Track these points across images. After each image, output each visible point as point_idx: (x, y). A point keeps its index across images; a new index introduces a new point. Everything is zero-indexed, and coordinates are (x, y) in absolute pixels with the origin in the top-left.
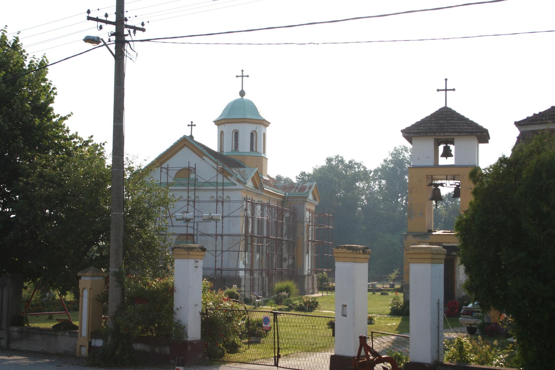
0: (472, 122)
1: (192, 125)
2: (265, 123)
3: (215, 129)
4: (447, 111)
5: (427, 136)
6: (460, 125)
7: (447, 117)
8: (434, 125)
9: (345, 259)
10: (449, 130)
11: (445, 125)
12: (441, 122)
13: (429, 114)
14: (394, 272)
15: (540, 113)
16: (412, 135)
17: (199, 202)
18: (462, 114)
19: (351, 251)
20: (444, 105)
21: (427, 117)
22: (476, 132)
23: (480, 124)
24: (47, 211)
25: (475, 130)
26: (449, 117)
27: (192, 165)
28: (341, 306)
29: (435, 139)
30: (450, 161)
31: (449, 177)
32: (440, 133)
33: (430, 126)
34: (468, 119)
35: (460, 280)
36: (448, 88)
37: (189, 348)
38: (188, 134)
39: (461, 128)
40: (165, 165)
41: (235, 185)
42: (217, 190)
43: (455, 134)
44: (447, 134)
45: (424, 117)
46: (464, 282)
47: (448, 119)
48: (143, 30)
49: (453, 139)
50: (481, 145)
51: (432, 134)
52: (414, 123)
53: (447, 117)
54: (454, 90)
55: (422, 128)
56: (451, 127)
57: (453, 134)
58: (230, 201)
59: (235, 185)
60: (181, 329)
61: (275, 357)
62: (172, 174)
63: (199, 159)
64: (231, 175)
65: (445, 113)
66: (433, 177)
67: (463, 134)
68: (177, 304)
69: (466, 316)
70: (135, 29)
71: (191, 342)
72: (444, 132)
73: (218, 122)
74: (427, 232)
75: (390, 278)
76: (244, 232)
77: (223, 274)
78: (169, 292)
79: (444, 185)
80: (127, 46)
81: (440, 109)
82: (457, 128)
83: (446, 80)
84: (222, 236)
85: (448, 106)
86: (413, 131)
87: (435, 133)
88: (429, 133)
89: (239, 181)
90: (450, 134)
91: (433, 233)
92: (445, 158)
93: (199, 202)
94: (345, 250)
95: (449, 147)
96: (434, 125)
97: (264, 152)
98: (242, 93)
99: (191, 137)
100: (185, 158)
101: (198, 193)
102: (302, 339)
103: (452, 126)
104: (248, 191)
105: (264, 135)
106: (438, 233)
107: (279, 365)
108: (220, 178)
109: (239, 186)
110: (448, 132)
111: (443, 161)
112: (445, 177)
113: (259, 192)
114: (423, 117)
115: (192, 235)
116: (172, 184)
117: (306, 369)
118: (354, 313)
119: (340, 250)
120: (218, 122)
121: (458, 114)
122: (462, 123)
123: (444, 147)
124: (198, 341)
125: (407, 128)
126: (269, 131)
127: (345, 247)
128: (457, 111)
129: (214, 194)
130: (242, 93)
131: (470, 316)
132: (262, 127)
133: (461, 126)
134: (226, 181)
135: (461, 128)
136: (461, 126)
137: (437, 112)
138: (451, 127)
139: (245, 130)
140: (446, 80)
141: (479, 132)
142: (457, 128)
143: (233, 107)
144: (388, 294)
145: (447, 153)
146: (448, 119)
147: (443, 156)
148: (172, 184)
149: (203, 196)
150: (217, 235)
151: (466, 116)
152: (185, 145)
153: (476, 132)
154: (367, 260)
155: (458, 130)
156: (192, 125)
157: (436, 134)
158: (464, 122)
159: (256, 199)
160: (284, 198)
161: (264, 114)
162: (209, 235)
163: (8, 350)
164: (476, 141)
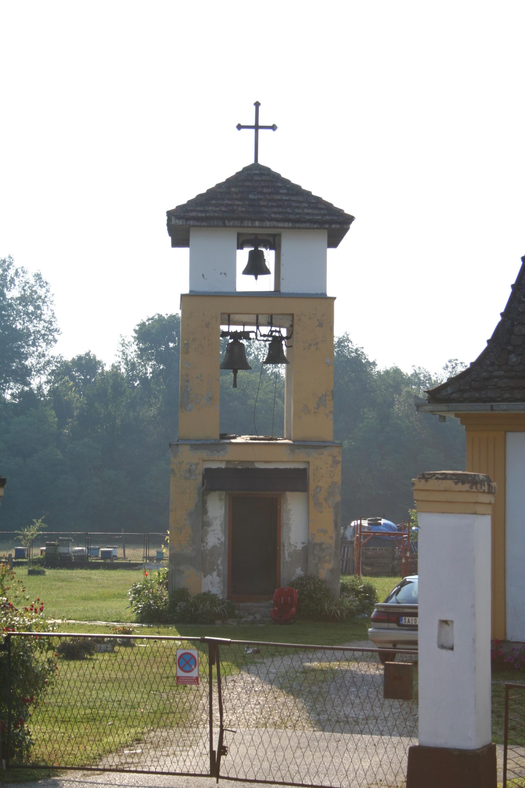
0: (319, 200)
4: (261, 175)
5: (225, 226)
6: (294, 204)
7: (263, 187)
8: (237, 203)
9: (447, 506)
10: (273, 216)
11: (262, 203)
12: (251, 196)
14: (33, 524)
16: (191, 223)
18: (294, 181)
19: (467, 487)
20: (252, 161)
21: (219, 186)
22: (331, 222)
23: (337, 204)
25: (327, 218)
26: (268, 187)
28: (436, 624)
29: (239, 235)
30: (265, 283)
31: (262, 319)
32: (254, 220)
33: (228, 205)
34: (308, 194)
35: (292, 541)
36: (253, 124)
39: (297, 211)
43: (286, 225)
44: (268, 224)
45: (213, 185)
46: (300, 547)
47: (265, 190)
49: (279, 235)
50: (330, 251)
51: (237, 223)
52: (193, 196)
53: (263, 187)
54: (274, 128)
55: (214, 209)
56: (276, 210)
57: (281, 225)
61: (212, 752)
65: (256, 178)
66: (232, 317)
67: (303, 225)
69: (385, 625)
72: (262, 220)
74: (218, 437)
75: (25, 536)
77: (122, 550)
79: (252, 335)
81: (245, 169)
82: (289, 210)
83: (257, 104)
85: (262, 162)
86: (194, 214)
87: (242, 219)
88: (230, 219)
90: (275, 224)
91: (233, 441)
92: (252, 277)
94: (448, 484)
95: (262, 252)
96: (237, 203)
102: (168, 699)
103: (278, 206)
106: (239, 440)
107: (221, 774)
110: (271, 220)
111: (246, 284)
112: (253, 318)
114: (212, 185)
117: (345, 784)
118: (474, 641)
119: (433, 484)
121: (287, 182)
122: (298, 202)
123: (251, 252)
125: (180, 208)
127: (445, 477)
128: (284, 175)
131: (394, 625)
133: (297, 207)
135: (297, 211)
136: (297, 207)
137: (238, 174)
138: (276, 210)
140: (257, 104)
141: (336, 222)
142: (289, 210)
144: (43, 573)
145: (256, 267)
146: (265, 190)
147: (248, 271)
151: (305, 187)
153: (331, 222)
154: (489, 509)
155: (292, 217)
157: (246, 223)
158: (301, 199)
164: (326, 243)
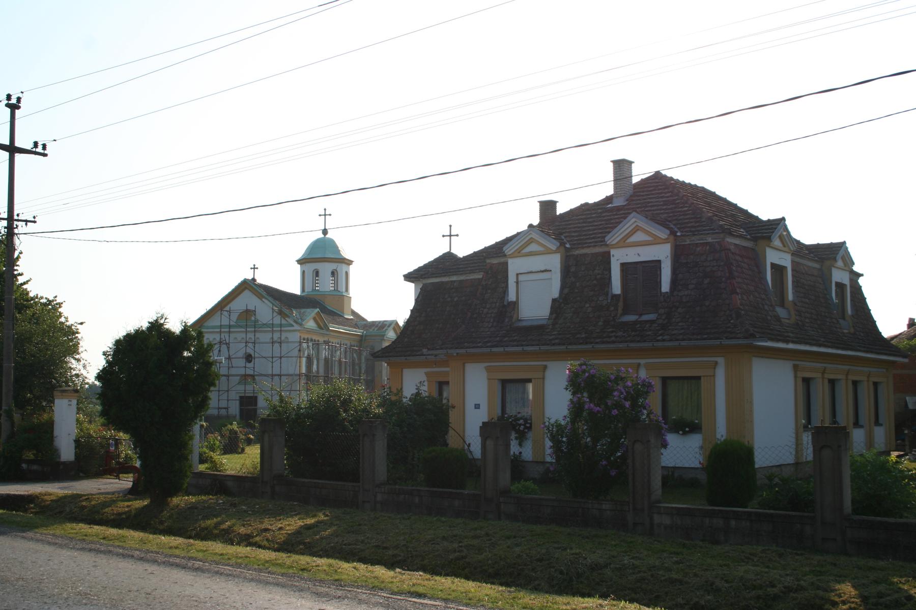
1: (254, 268)
2: (349, 262)
3: (298, 268)
13: (432, 259)
15: (769, 220)
17: (259, 343)
24: (185, 354)
27: (251, 308)
37: (61, 467)
38: (250, 277)
40: (227, 308)
41: (292, 326)
42: (273, 332)
48: (35, 222)
58: (288, 342)
59: (292, 326)
60: (56, 452)
62: (234, 317)
63: (259, 301)
64: (288, 317)
68: (56, 433)
70: (26, 221)
71: (64, 463)
73: (301, 262)
76: (304, 370)
78: (51, 424)
80: (15, 238)
84: (280, 376)
89: (295, 322)
93: (259, 343)
97: (347, 290)
98: (325, 232)
99: (254, 280)
100: (248, 300)
101: (257, 335)
104: (309, 331)
105: (347, 274)
108: (277, 320)
109: (296, 327)
113: (324, 332)
115: (253, 376)
116: (234, 326)
120: (301, 262)
124: (71, 462)
126: (352, 269)
129: (244, 335)
130: (325, 232)
132: (344, 266)
134: (284, 322)
139: (326, 269)
143: (316, 246)
148: (234, 326)
149: (264, 337)
150: (273, 375)
152: (246, 288)
156: (254, 268)
159: (321, 340)
160: (361, 336)
161: (346, 254)
162: (265, 375)
163: (910, 598)
